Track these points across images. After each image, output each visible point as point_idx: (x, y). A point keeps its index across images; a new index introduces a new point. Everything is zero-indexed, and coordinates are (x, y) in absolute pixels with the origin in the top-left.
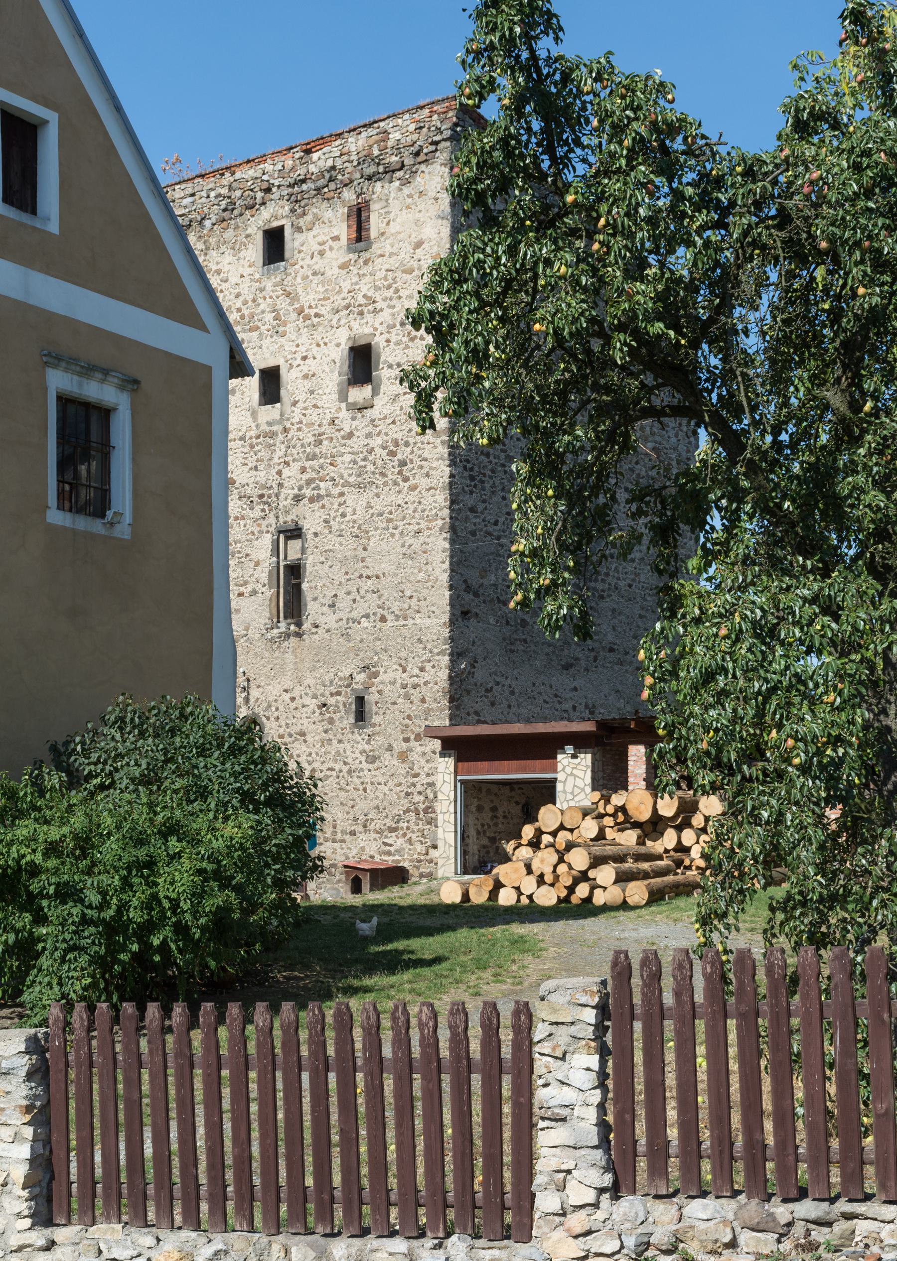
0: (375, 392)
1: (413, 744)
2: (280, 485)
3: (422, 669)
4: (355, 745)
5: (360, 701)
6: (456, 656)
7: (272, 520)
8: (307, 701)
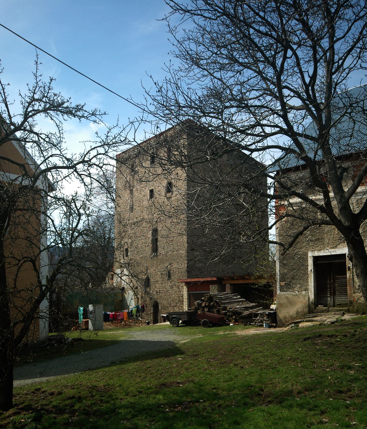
0: (172, 194)
1: (180, 284)
2: (153, 218)
3: (182, 264)
4: (168, 284)
5: (169, 272)
6: (189, 261)
7: (152, 227)
8: (158, 273)
